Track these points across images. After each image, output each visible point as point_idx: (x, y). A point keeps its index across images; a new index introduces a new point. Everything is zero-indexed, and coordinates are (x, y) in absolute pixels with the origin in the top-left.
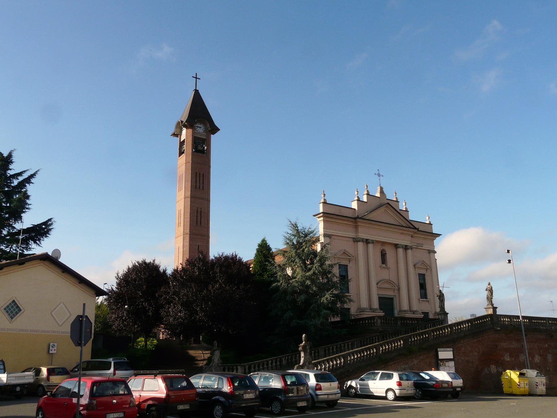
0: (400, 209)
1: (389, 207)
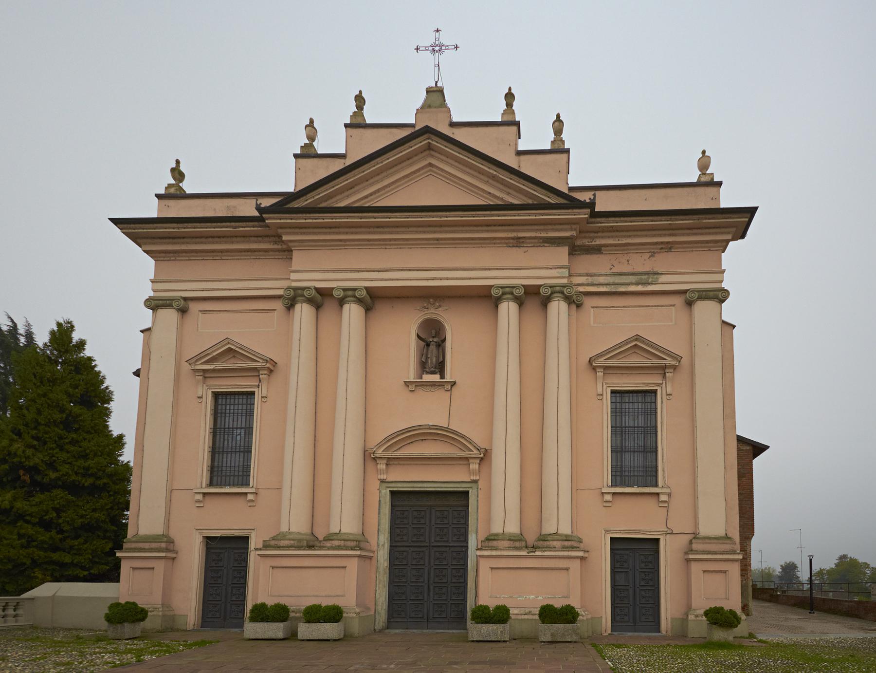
0: (724, 318)
1: (436, 143)
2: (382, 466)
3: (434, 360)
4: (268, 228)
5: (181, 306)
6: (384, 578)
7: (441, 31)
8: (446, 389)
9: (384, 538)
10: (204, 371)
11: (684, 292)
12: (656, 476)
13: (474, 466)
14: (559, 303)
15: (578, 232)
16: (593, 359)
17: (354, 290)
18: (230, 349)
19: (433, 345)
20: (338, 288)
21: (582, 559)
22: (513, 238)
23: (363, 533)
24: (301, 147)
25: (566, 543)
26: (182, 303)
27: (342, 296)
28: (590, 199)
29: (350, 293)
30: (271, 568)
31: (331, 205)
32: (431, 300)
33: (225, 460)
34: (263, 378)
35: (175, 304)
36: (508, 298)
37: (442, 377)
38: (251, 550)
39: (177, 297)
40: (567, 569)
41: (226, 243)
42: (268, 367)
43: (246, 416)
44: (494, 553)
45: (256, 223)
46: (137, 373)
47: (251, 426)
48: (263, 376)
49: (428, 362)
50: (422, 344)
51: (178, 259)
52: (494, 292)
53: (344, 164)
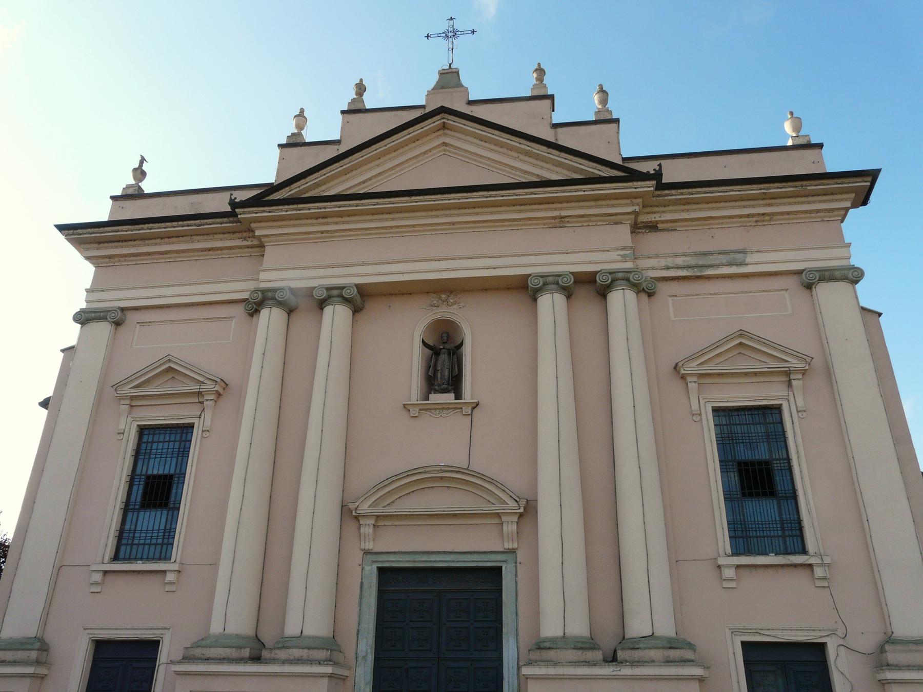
0: (863, 304)
1: (451, 121)
4: (239, 224)
5: (117, 318)
8: (464, 413)
9: (367, 645)
11: (800, 272)
12: (801, 536)
15: (641, 206)
16: (680, 364)
17: (342, 288)
18: (170, 369)
21: (701, 680)
22: (555, 218)
23: (334, 636)
25: (673, 654)
27: (325, 297)
28: (654, 170)
29: (335, 292)
32: (443, 296)
34: (207, 405)
37: (458, 396)
38: (161, 663)
41: (107, 248)
42: (217, 391)
43: (177, 457)
44: (551, 671)
46: (45, 404)
49: (437, 377)
52: (532, 283)
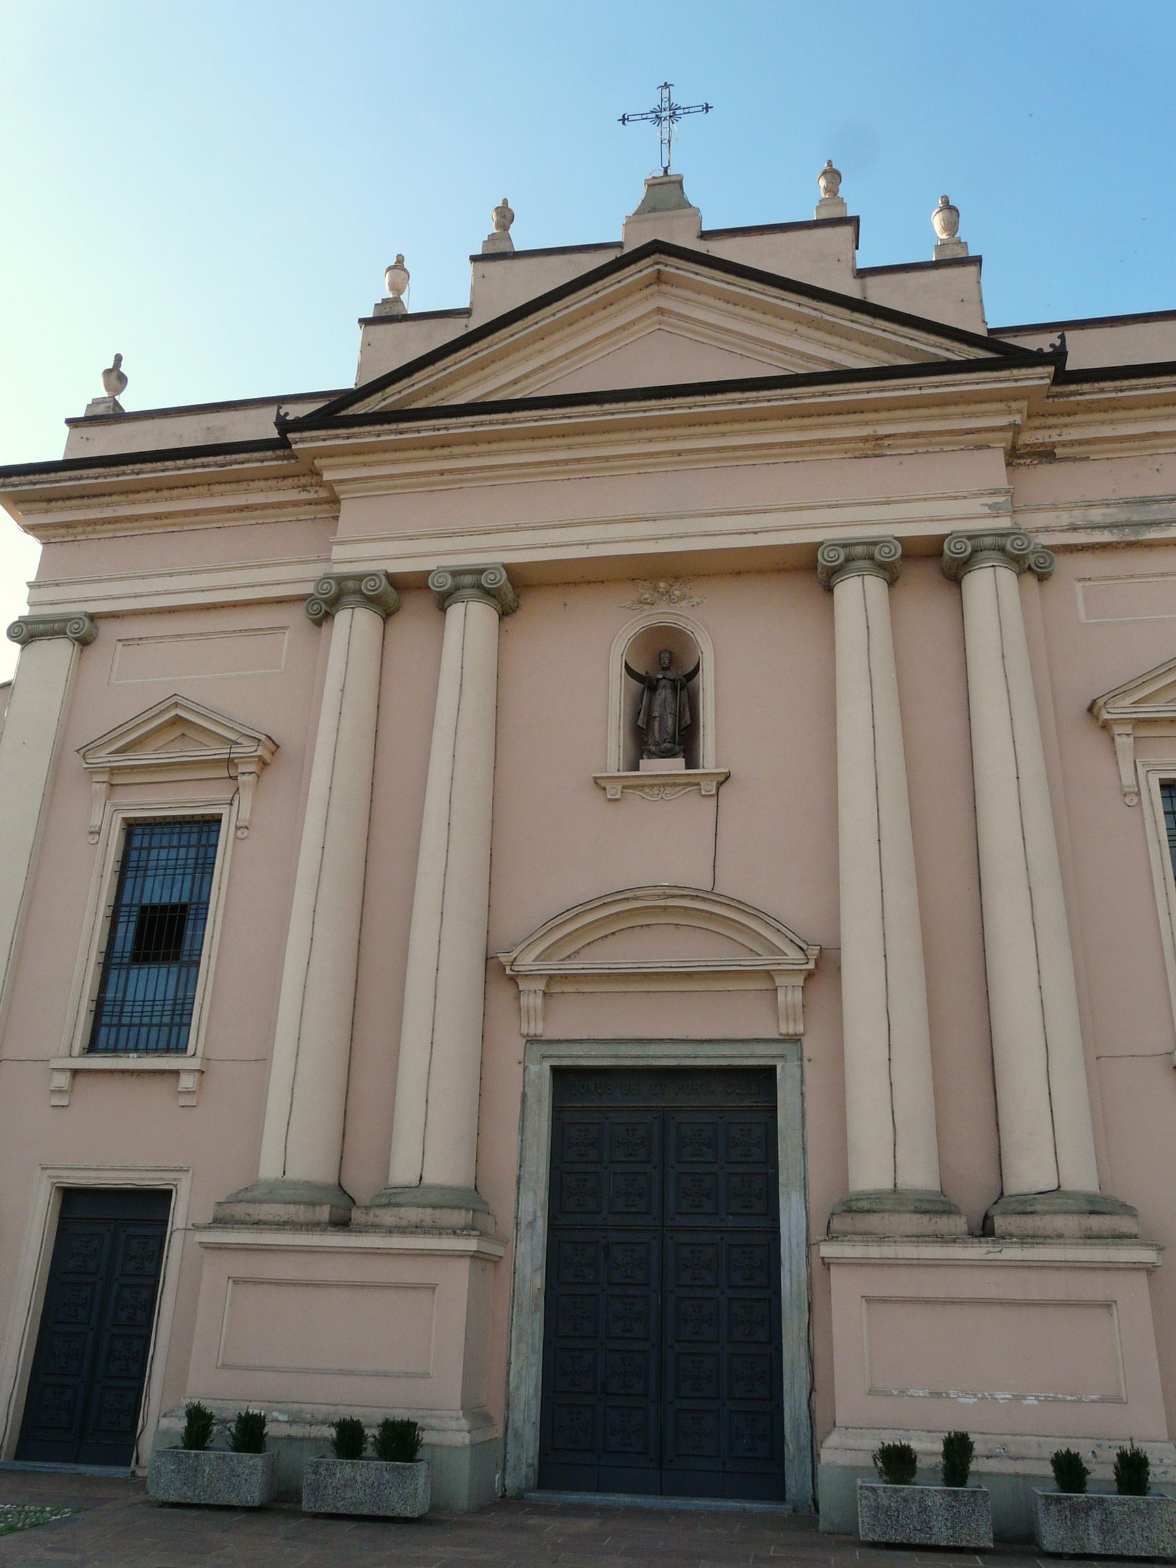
1: (673, 267)
2: (531, 1001)
3: (670, 721)
5: (84, 631)
6: (533, 1326)
7: (672, 85)
10: (114, 771)
13: (790, 996)
14: (995, 571)
16: (1101, 702)
17: (480, 572)
18: (178, 720)
19: (665, 687)
20: (440, 570)
21: (1150, 1270)
22: (865, 439)
23: (476, 1186)
24: (377, 305)
25: (1097, 1223)
26: (86, 626)
28: (1052, 346)
30: (231, 1282)
31: (439, 404)
32: (662, 585)
33: (132, 985)
34: (244, 783)
35: (70, 627)
36: (859, 569)
38: (174, 1228)
39: (77, 613)
40: (1108, 1305)
42: (260, 757)
45: (269, 454)
47: (203, 899)
48: (245, 777)
50: (635, 685)
51: (91, 537)
52: (824, 558)
53: (466, 326)
